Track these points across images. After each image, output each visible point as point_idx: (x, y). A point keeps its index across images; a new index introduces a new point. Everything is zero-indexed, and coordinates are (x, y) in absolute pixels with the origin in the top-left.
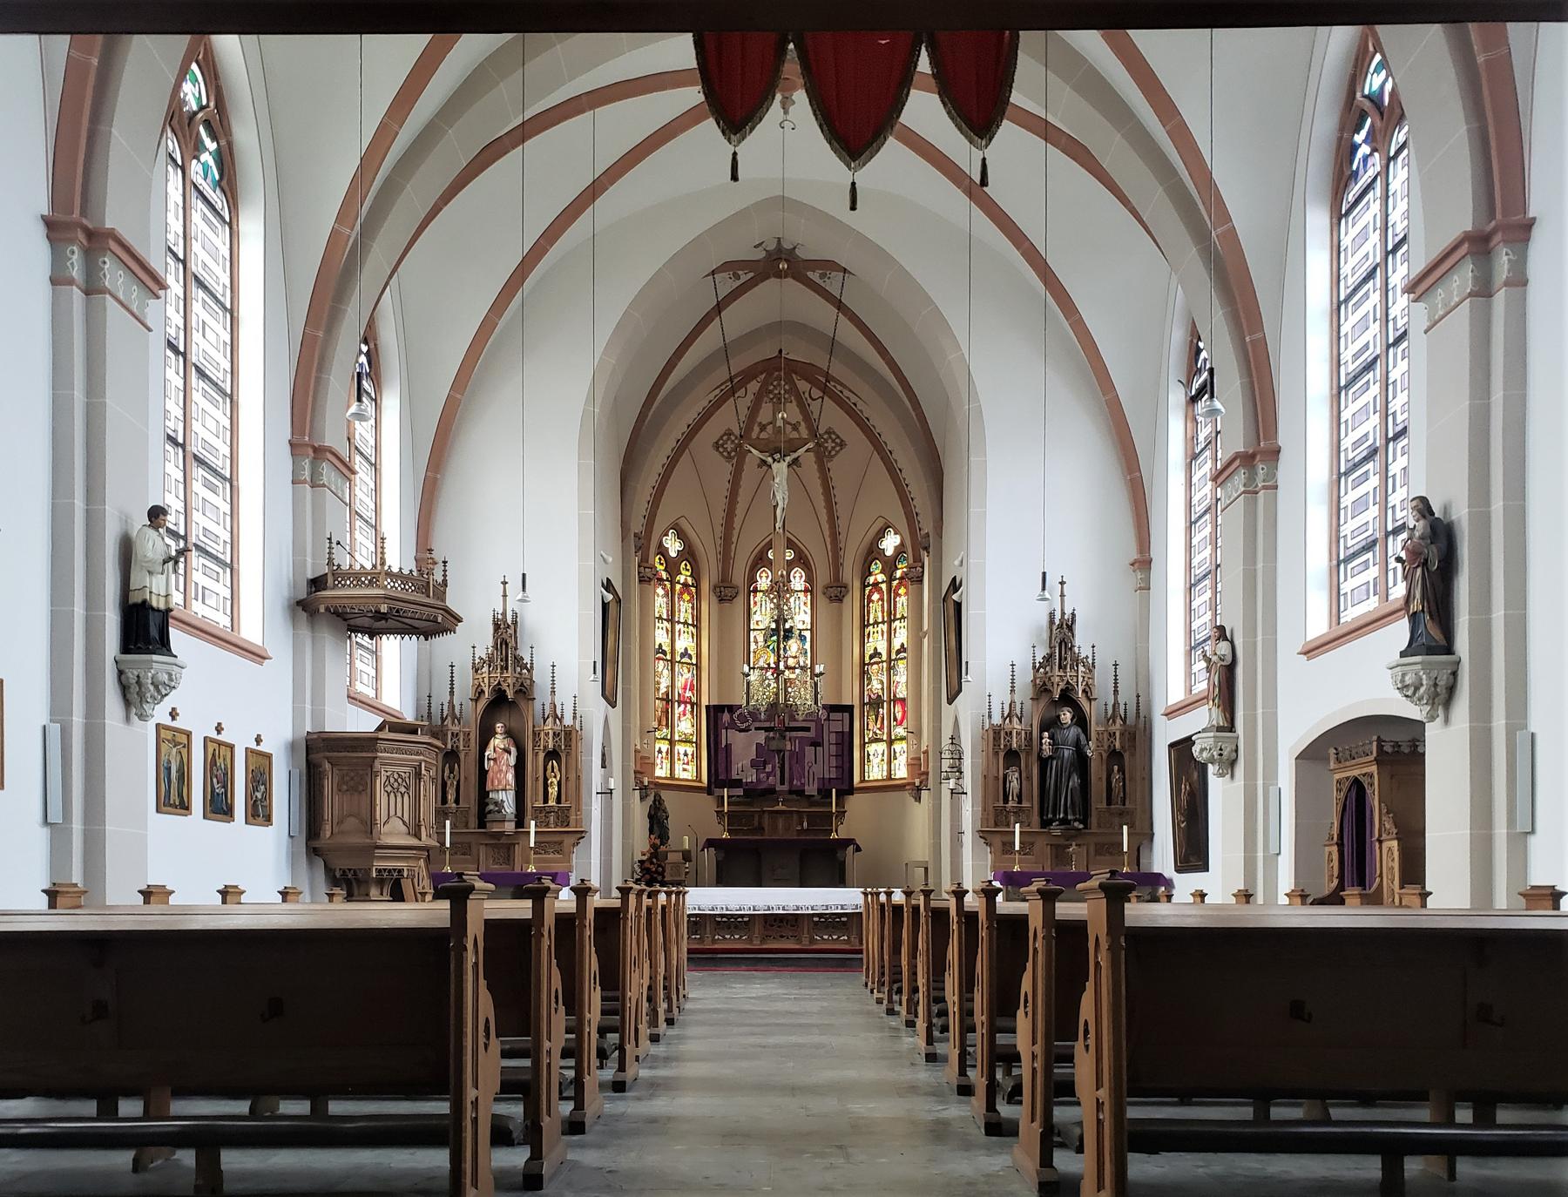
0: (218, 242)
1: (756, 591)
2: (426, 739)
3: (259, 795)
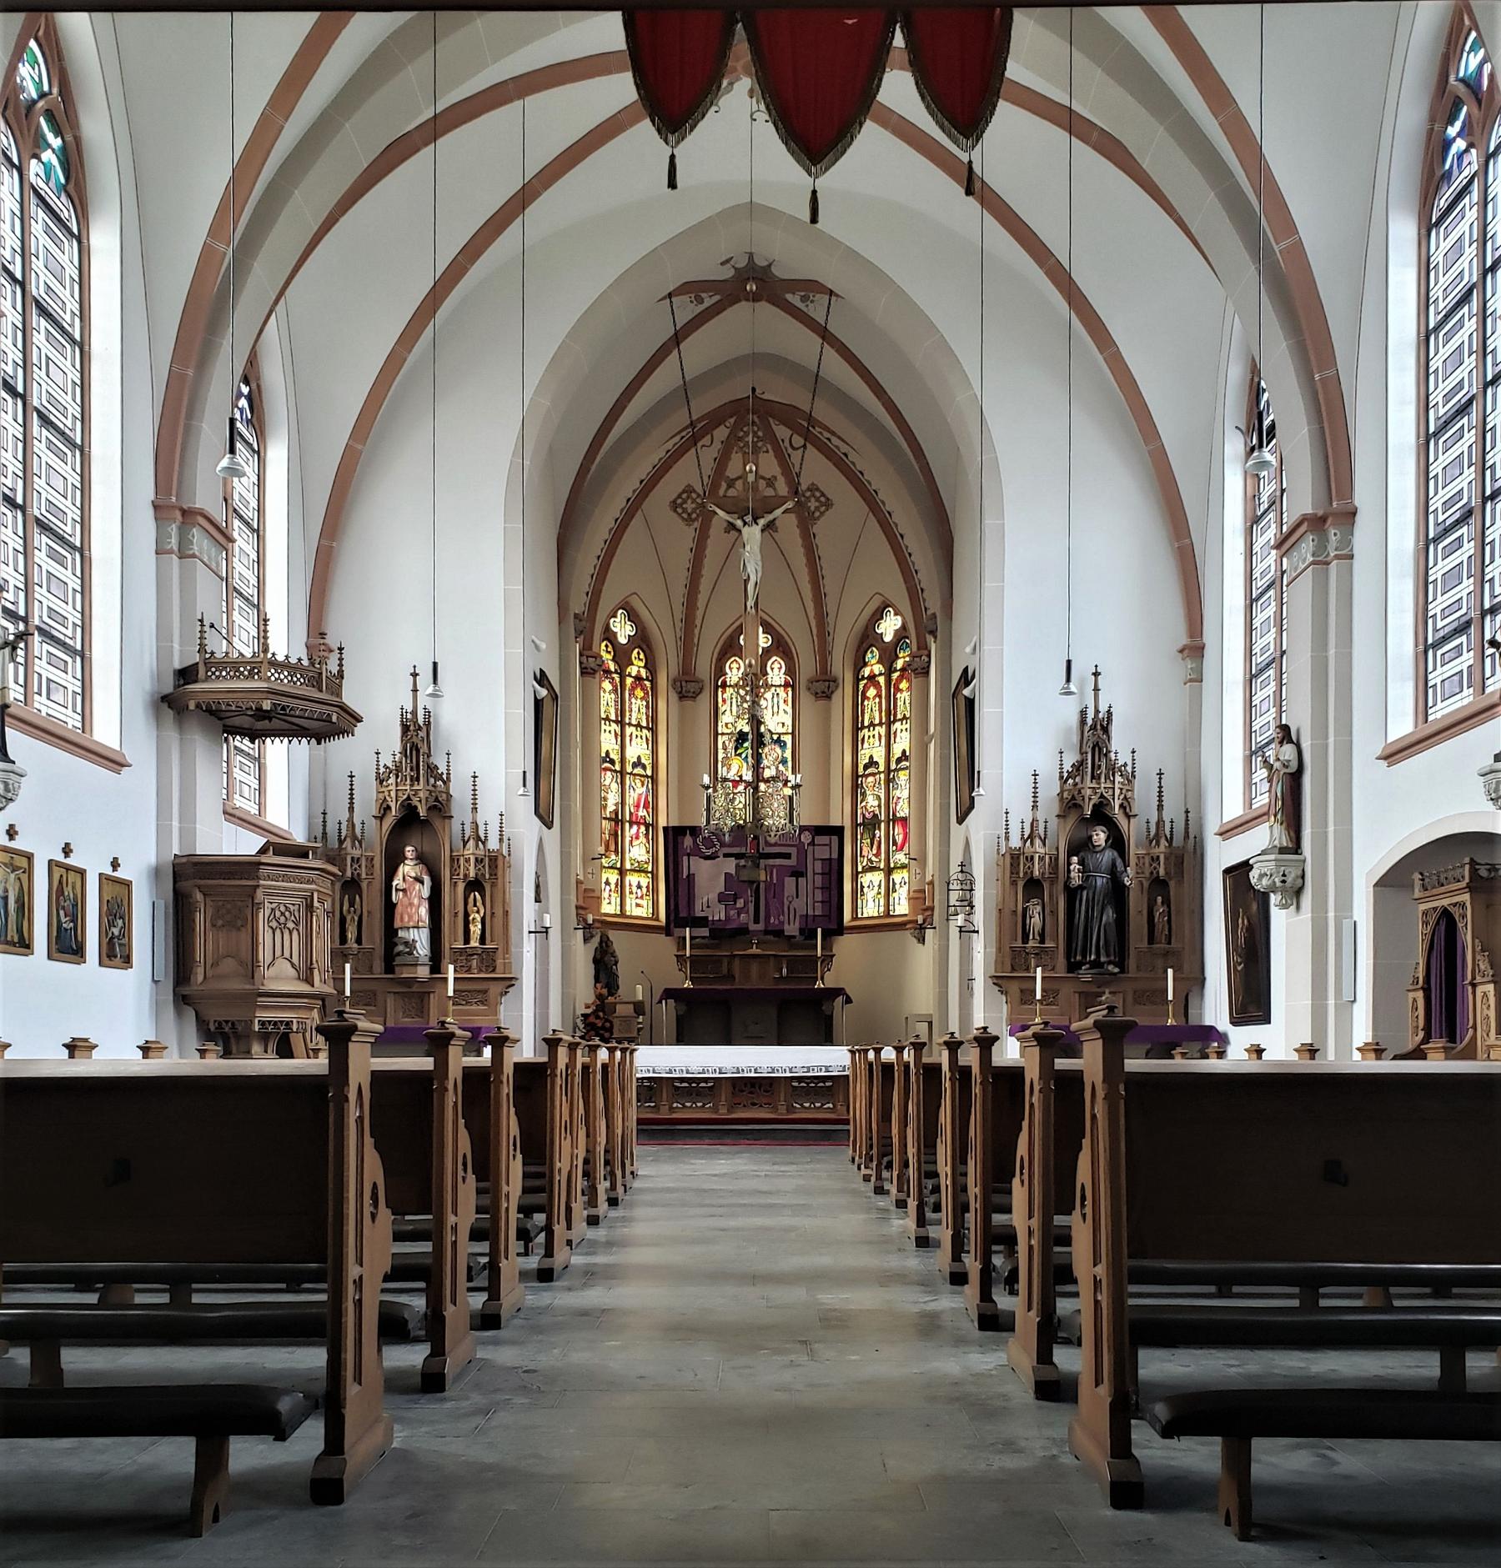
0: (64, 259)
1: (724, 686)
2: (318, 864)
3: (116, 931)
